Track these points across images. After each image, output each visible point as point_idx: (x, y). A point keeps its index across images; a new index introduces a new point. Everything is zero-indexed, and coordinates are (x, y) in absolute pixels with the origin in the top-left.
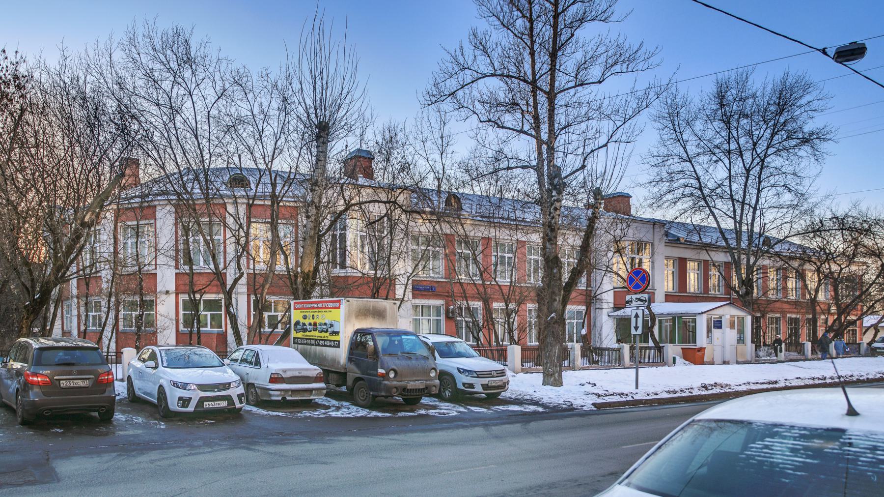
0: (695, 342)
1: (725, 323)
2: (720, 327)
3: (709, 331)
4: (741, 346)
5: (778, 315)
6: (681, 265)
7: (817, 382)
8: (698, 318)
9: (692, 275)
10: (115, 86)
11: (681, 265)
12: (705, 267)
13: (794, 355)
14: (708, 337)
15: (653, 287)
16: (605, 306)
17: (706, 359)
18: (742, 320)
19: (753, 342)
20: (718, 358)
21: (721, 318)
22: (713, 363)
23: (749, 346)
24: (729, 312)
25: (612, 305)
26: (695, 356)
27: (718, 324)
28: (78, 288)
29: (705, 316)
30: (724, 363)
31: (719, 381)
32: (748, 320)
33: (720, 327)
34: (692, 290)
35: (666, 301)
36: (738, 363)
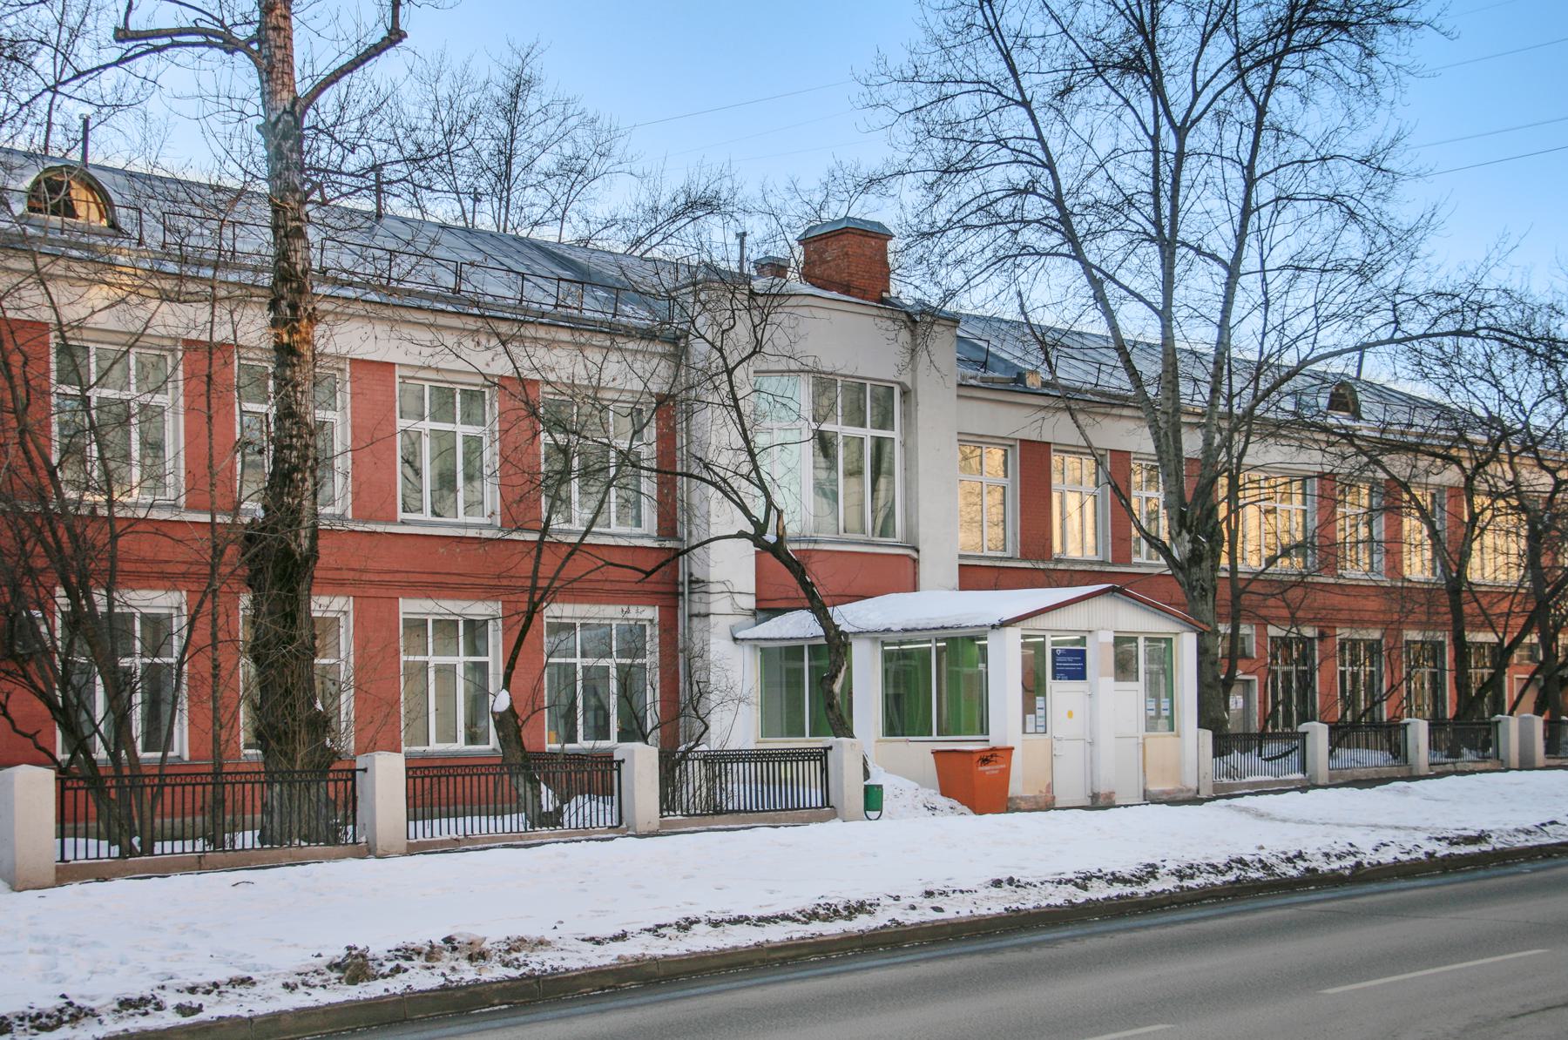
0: (984, 729)
1: (1099, 657)
2: (1080, 674)
3: (1033, 687)
4: (1161, 741)
5: (1375, 634)
6: (1034, 463)
7: (1100, 891)
8: (993, 642)
9: (1073, 501)
10: (1288, 404)
11: (1034, 463)
12: (1115, 474)
13: (1373, 759)
14: (1029, 708)
15: (911, 531)
16: (719, 604)
17: (1016, 788)
18: (1162, 649)
19: (1203, 723)
20: (1070, 786)
21: (1083, 641)
22: (1047, 805)
23: (1193, 742)
24: (1105, 621)
25: (750, 603)
26: (976, 783)
27: (1073, 664)
28: (253, 622)
29: (1013, 635)
30: (1099, 802)
31: (464, 930)
32: (1187, 646)
33: (1080, 674)
34: (1073, 552)
35: (964, 585)
36: (1150, 799)
